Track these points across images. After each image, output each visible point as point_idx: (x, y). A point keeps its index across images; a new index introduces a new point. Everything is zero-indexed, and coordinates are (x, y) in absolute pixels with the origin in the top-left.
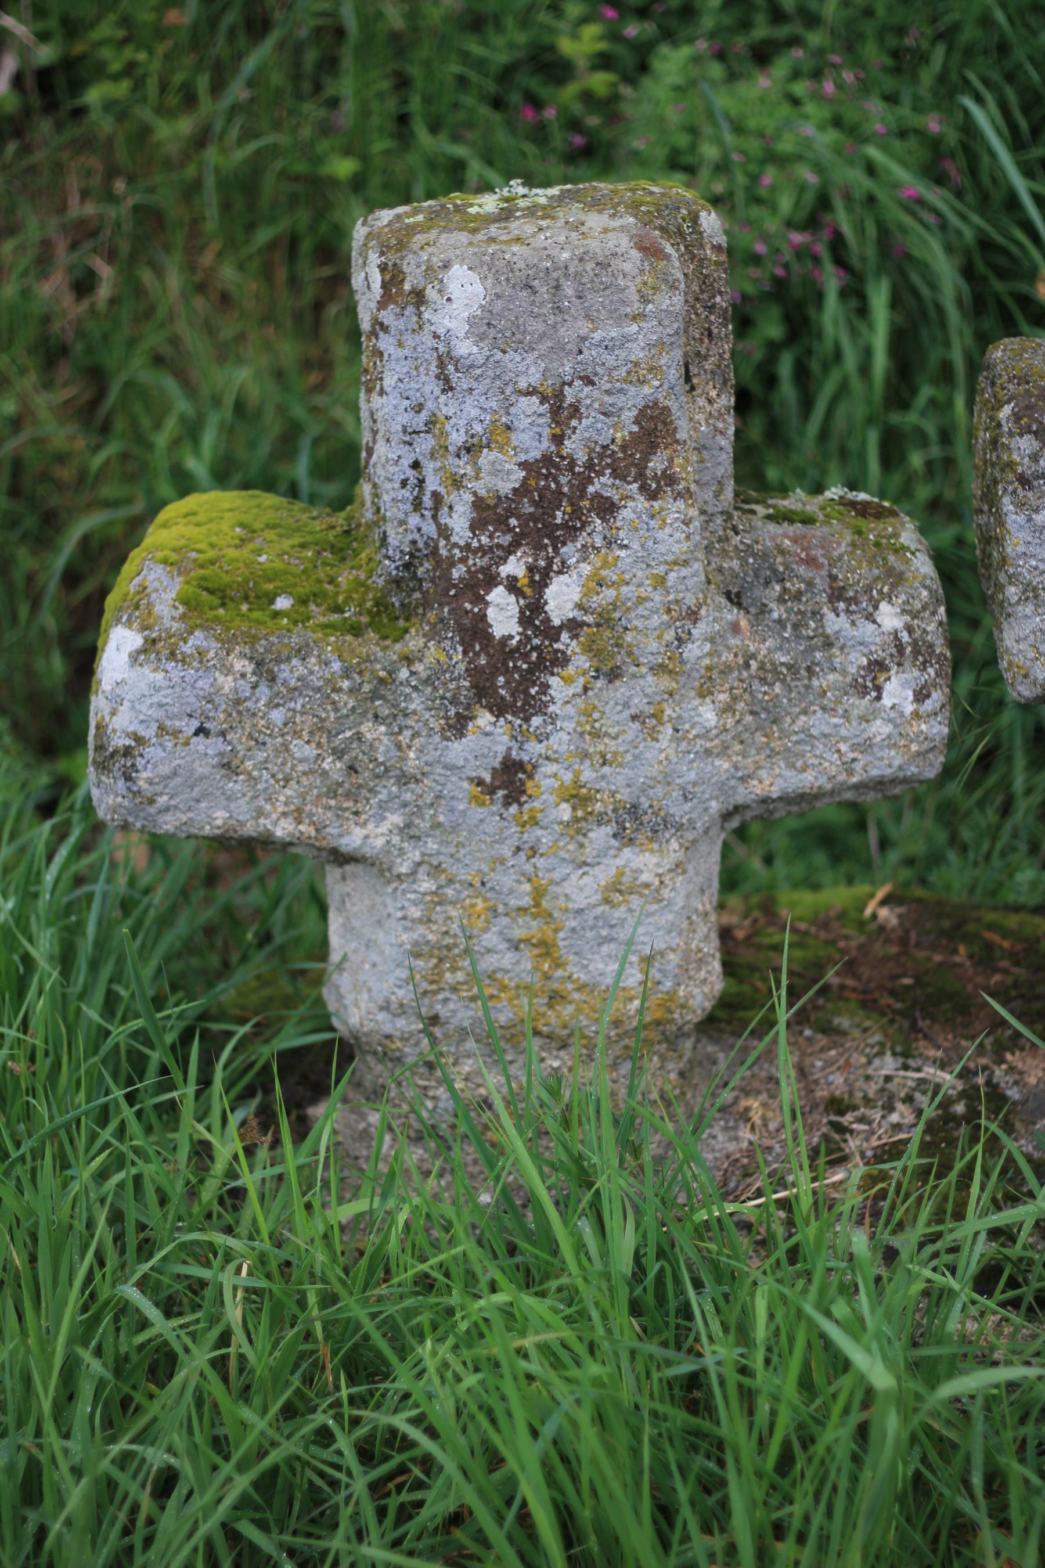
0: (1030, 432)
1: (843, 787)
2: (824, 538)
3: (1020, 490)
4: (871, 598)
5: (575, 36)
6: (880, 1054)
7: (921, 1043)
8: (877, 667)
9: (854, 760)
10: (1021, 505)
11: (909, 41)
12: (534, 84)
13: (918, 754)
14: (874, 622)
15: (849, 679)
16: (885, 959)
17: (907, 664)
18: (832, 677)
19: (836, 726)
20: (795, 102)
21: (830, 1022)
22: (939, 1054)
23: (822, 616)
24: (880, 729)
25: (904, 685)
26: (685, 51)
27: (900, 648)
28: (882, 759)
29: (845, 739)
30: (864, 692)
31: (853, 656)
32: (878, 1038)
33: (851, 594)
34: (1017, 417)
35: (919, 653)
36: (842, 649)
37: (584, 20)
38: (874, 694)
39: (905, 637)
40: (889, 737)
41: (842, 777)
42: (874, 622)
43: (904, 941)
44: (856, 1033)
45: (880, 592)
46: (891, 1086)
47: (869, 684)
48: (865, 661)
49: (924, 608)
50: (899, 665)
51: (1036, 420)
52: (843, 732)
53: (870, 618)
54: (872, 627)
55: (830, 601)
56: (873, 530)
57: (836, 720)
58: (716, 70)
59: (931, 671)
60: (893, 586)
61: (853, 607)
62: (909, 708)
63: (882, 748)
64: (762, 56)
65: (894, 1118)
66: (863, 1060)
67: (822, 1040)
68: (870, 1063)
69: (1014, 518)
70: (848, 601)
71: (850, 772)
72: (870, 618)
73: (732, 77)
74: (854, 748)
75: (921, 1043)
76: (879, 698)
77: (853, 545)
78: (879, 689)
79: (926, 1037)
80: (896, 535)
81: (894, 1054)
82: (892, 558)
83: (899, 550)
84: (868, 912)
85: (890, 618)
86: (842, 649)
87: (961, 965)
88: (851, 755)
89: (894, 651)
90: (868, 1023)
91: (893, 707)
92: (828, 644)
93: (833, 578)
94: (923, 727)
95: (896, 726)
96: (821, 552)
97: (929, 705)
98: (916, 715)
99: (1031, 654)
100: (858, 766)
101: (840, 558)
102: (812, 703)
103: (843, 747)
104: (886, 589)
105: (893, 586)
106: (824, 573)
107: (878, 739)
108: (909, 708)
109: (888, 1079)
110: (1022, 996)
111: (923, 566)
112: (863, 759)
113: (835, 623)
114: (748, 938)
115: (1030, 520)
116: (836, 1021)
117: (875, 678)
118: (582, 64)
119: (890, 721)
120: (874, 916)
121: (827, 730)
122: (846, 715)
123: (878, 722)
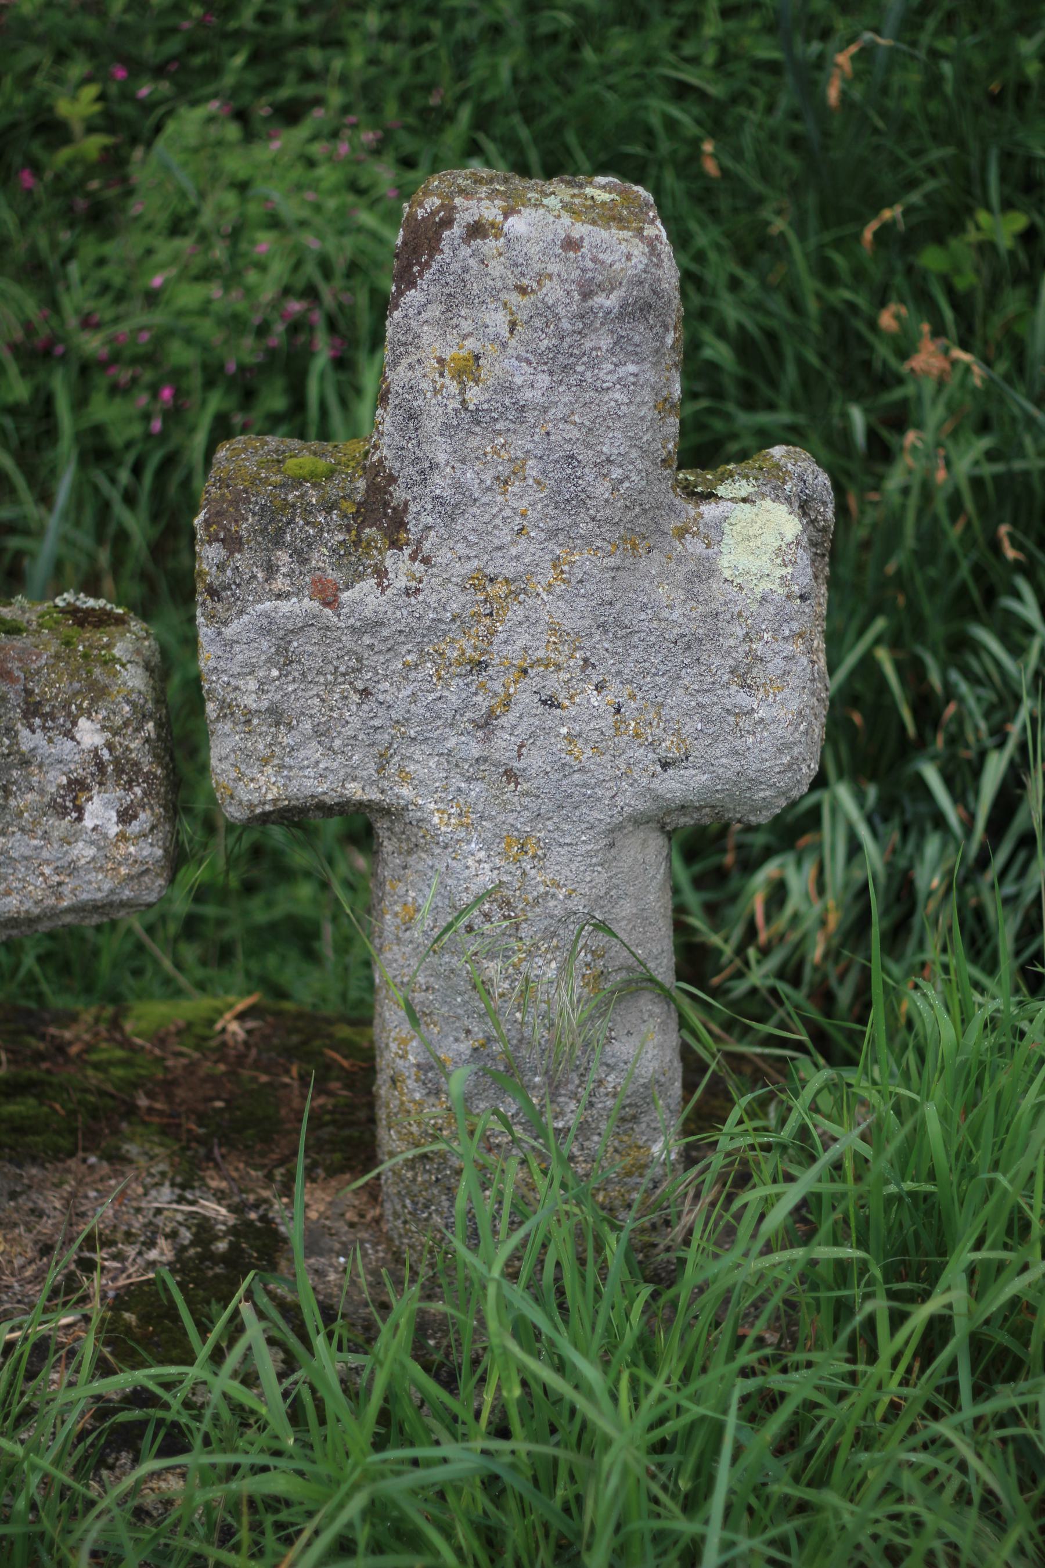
0: (218, 540)
1: (53, 914)
2: (24, 650)
3: (208, 602)
4: (69, 714)
5: (74, 99)
6: (158, 1185)
7: (209, 1173)
8: (77, 786)
9: (60, 884)
10: (211, 617)
11: (434, 101)
12: (36, 148)
13: (130, 877)
14: (73, 738)
15: (47, 799)
16: (210, 1078)
17: (109, 784)
18: (29, 796)
19: (36, 848)
20: (311, 163)
21: (119, 1149)
22: (224, 1185)
23: (17, 733)
24: (83, 851)
25: (106, 805)
26: (201, 112)
27: (101, 766)
28: (90, 882)
29: (47, 862)
30: (63, 812)
31: (50, 776)
32: (163, 1167)
33: (47, 709)
34: (207, 524)
35: (123, 771)
36: (40, 766)
37: (87, 80)
38: (74, 815)
39: (106, 755)
40: (93, 859)
41: (51, 901)
42: (73, 738)
43: (241, 1059)
44: (142, 1162)
45: (79, 707)
46: (159, 1221)
47: (69, 804)
48: (64, 780)
49: (126, 724)
50: (101, 784)
51: (224, 528)
52: (45, 854)
53: (69, 735)
54: (70, 744)
55: (25, 717)
56: (86, 639)
57: (36, 842)
58: (232, 131)
59: (138, 791)
60: (93, 701)
61: (50, 724)
62: (113, 830)
63: (88, 872)
64: (290, 114)
65: (153, 1255)
66: (140, 1190)
67: (105, 1168)
68: (146, 1194)
69: (205, 632)
70: (44, 716)
71: (60, 897)
72: (69, 735)
73: (249, 136)
74: (58, 871)
75: (211, 1172)
76: (80, 819)
77: (57, 657)
78: (80, 810)
79: (217, 1167)
80: (109, 646)
81: (173, 1185)
82: (97, 671)
83: (108, 662)
84: (219, 1026)
85: (89, 734)
86: (40, 766)
87: (286, 1086)
88: (56, 879)
89: (93, 769)
90: (158, 1150)
91: (95, 829)
92: (25, 763)
93: (29, 692)
94: (132, 849)
95: (99, 849)
96: (17, 664)
97: (135, 827)
98: (122, 837)
99: (233, 775)
100: (66, 890)
101: (38, 671)
102: (9, 824)
103: (47, 871)
104: (85, 705)
105: (93, 701)
106: (19, 687)
107: (83, 861)
108: (113, 830)
109: (159, 1211)
110: (334, 1122)
111: (134, 679)
112: (70, 884)
113: (29, 740)
114: (79, 1055)
115: (219, 634)
116: (126, 1147)
117: (76, 798)
118: (78, 128)
119: (92, 843)
120: (224, 1030)
121: (28, 853)
122: (46, 836)
123: (81, 844)
